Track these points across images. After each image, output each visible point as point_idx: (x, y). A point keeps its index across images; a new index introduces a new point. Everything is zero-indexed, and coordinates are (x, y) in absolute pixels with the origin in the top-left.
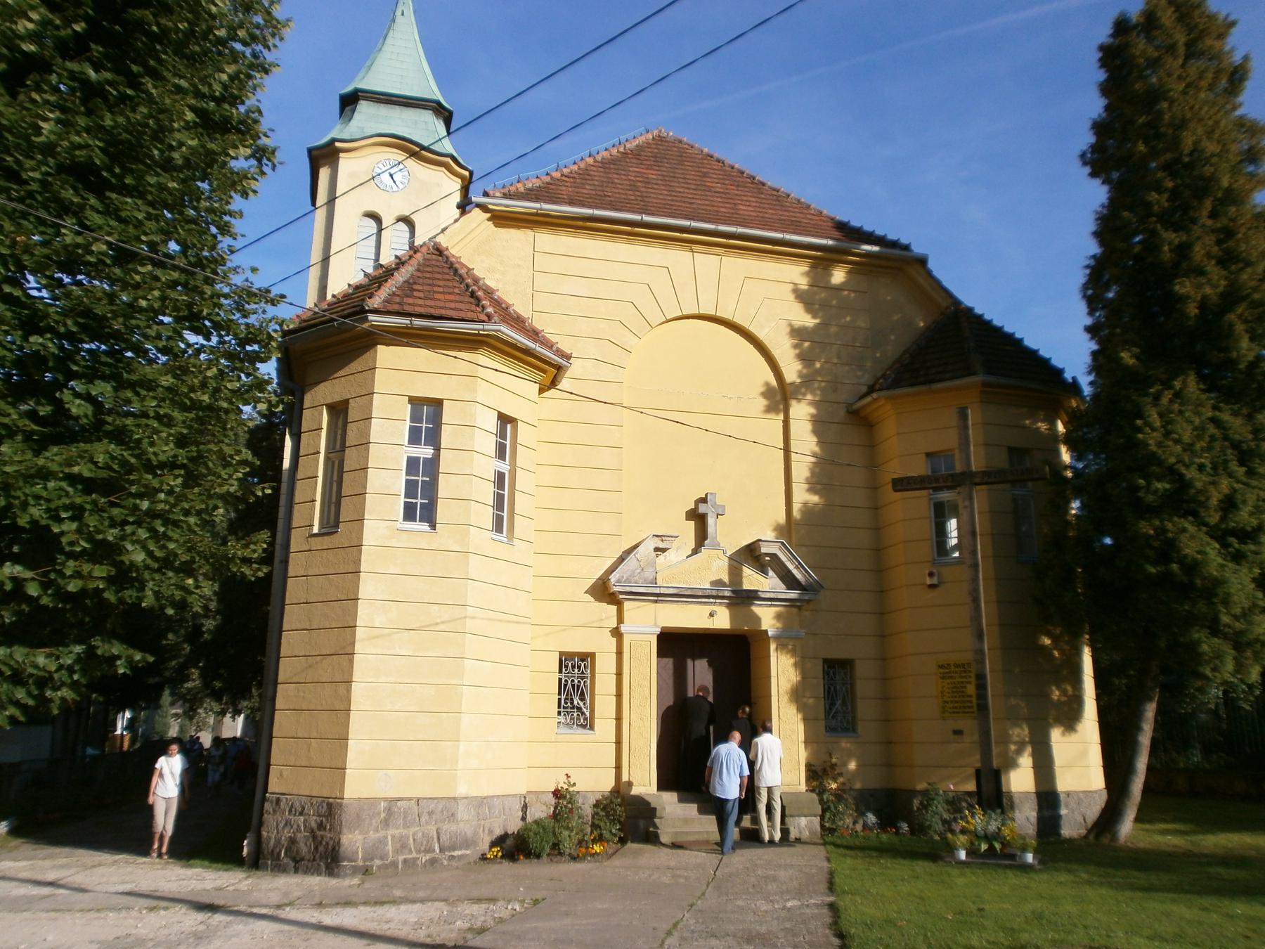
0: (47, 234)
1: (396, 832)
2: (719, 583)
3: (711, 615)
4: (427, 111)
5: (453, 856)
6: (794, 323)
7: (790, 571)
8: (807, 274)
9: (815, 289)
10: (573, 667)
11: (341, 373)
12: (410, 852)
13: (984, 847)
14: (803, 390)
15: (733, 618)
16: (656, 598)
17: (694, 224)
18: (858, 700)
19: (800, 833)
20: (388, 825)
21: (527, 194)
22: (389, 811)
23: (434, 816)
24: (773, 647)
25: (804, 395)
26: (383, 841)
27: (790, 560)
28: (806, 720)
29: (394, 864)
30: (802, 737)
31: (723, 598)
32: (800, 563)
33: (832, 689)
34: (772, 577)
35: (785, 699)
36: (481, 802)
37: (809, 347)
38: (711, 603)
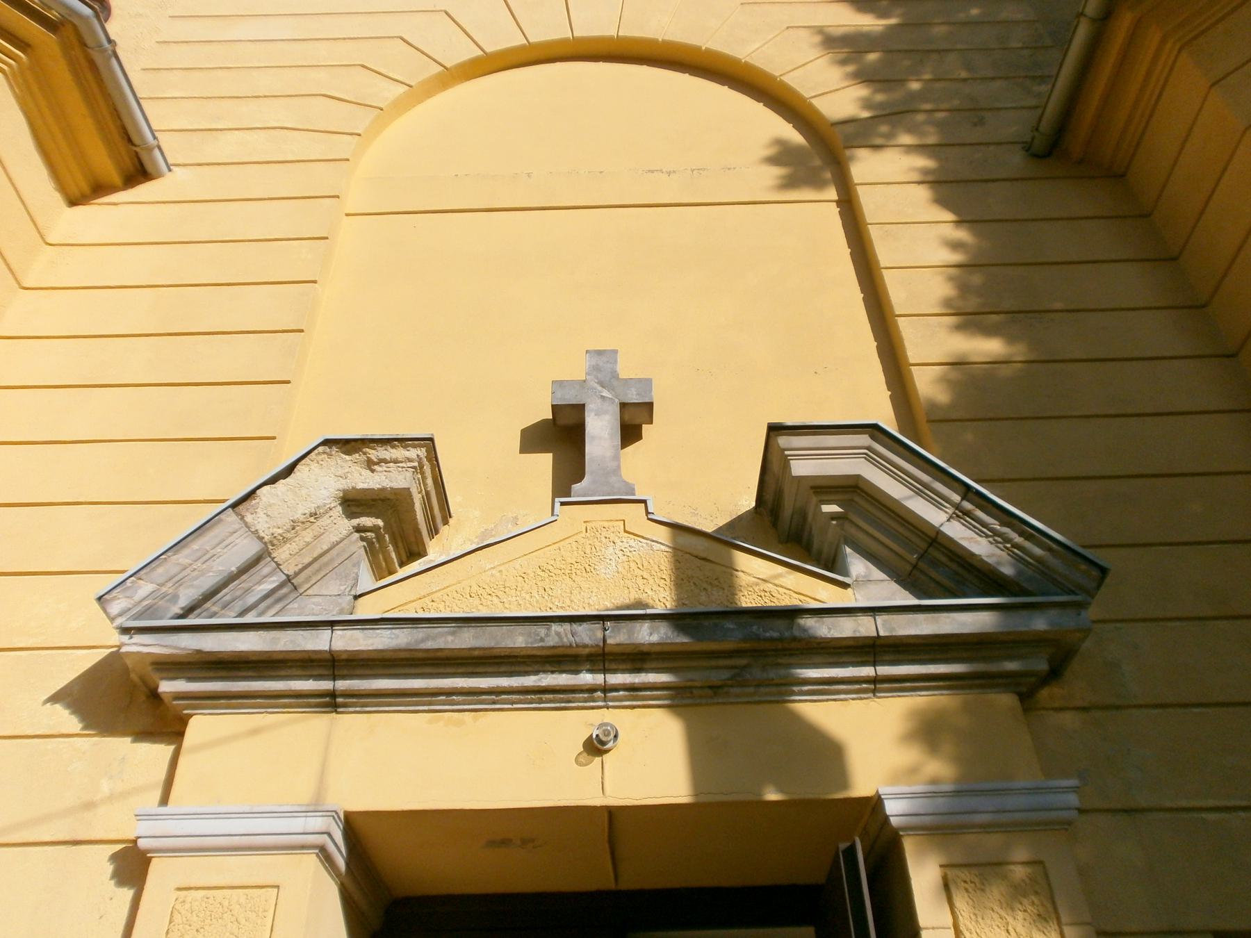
0: (314, 604)
3: (595, 747)
16: (326, 685)
27: (922, 490)
31: (637, 658)
32: (967, 491)
38: (591, 690)
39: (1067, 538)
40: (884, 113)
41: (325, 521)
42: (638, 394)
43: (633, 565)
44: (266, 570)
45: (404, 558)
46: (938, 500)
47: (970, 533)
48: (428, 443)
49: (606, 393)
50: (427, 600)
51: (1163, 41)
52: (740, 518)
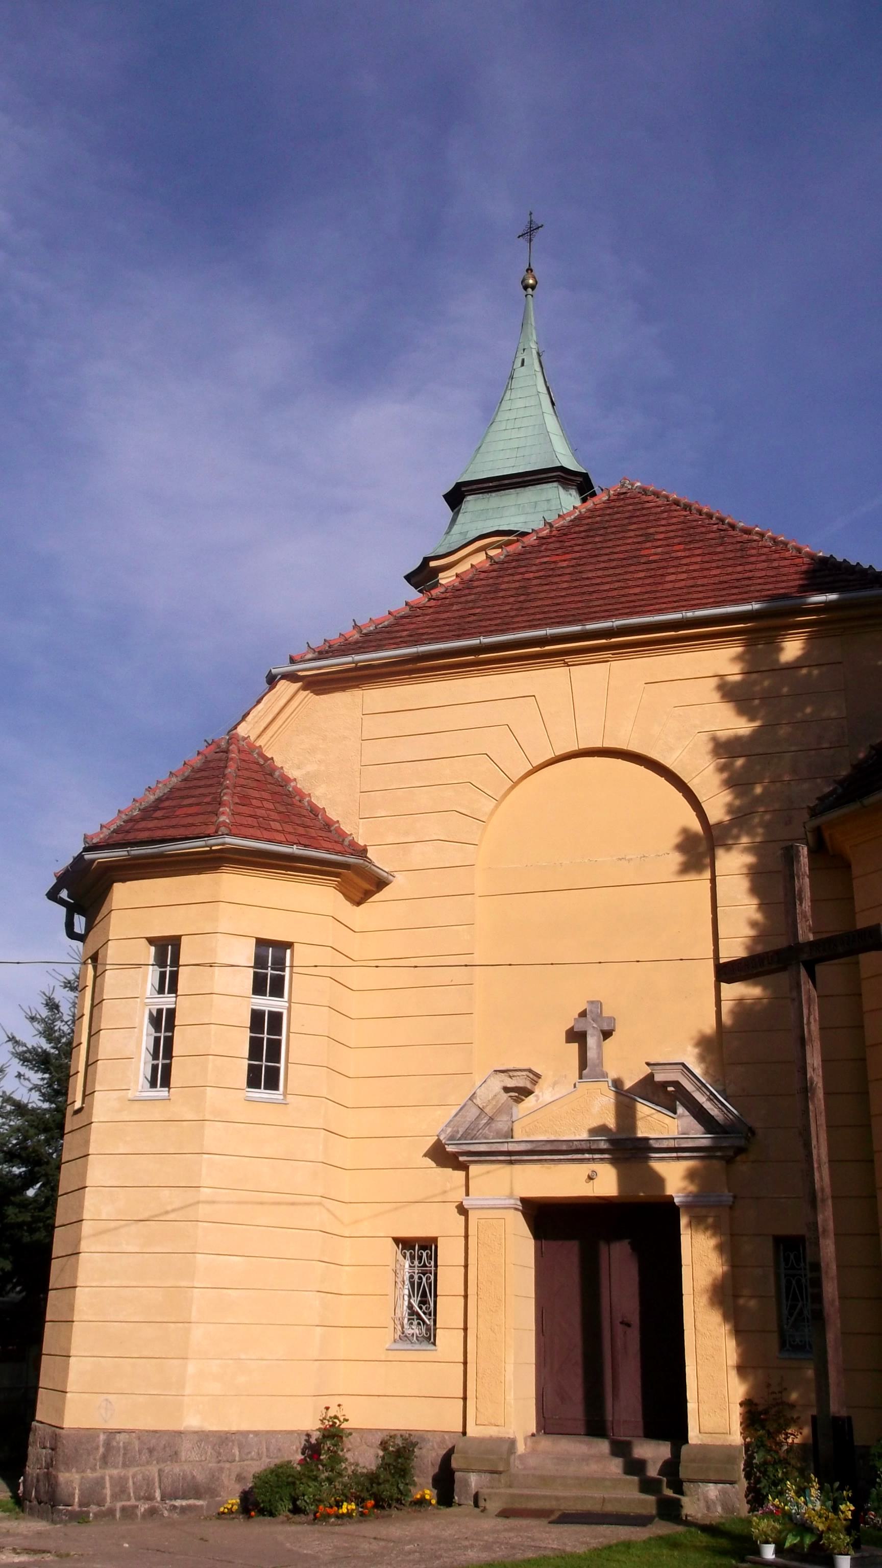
1: (115, 1472)
2: (602, 1130)
4: (550, 485)
5: (175, 1507)
6: (719, 734)
8: (739, 658)
9: (754, 676)
11: (98, 919)
12: (129, 1499)
14: (735, 831)
16: (508, 1158)
19: (708, 1508)
20: (106, 1463)
21: (364, 642)
22: (108, 1445)
23: (155, 1453)
24: (684, 1221)
25: (737, 837)
26: (100, 1482)
27: (699, 1089)
28: (739, 1333)
29: (111, 1512)
32: (711, 1093)
35: (704, 1300)
36: (223, 1440)
37: (744, 766)
38: (589, 1159)
40: (740, 815)
41: (499, 1096)
44: (483, 1116)
46: (703, 1094)
47: (712, 1107)
49: (595, 1025)
50: (536, 1123)
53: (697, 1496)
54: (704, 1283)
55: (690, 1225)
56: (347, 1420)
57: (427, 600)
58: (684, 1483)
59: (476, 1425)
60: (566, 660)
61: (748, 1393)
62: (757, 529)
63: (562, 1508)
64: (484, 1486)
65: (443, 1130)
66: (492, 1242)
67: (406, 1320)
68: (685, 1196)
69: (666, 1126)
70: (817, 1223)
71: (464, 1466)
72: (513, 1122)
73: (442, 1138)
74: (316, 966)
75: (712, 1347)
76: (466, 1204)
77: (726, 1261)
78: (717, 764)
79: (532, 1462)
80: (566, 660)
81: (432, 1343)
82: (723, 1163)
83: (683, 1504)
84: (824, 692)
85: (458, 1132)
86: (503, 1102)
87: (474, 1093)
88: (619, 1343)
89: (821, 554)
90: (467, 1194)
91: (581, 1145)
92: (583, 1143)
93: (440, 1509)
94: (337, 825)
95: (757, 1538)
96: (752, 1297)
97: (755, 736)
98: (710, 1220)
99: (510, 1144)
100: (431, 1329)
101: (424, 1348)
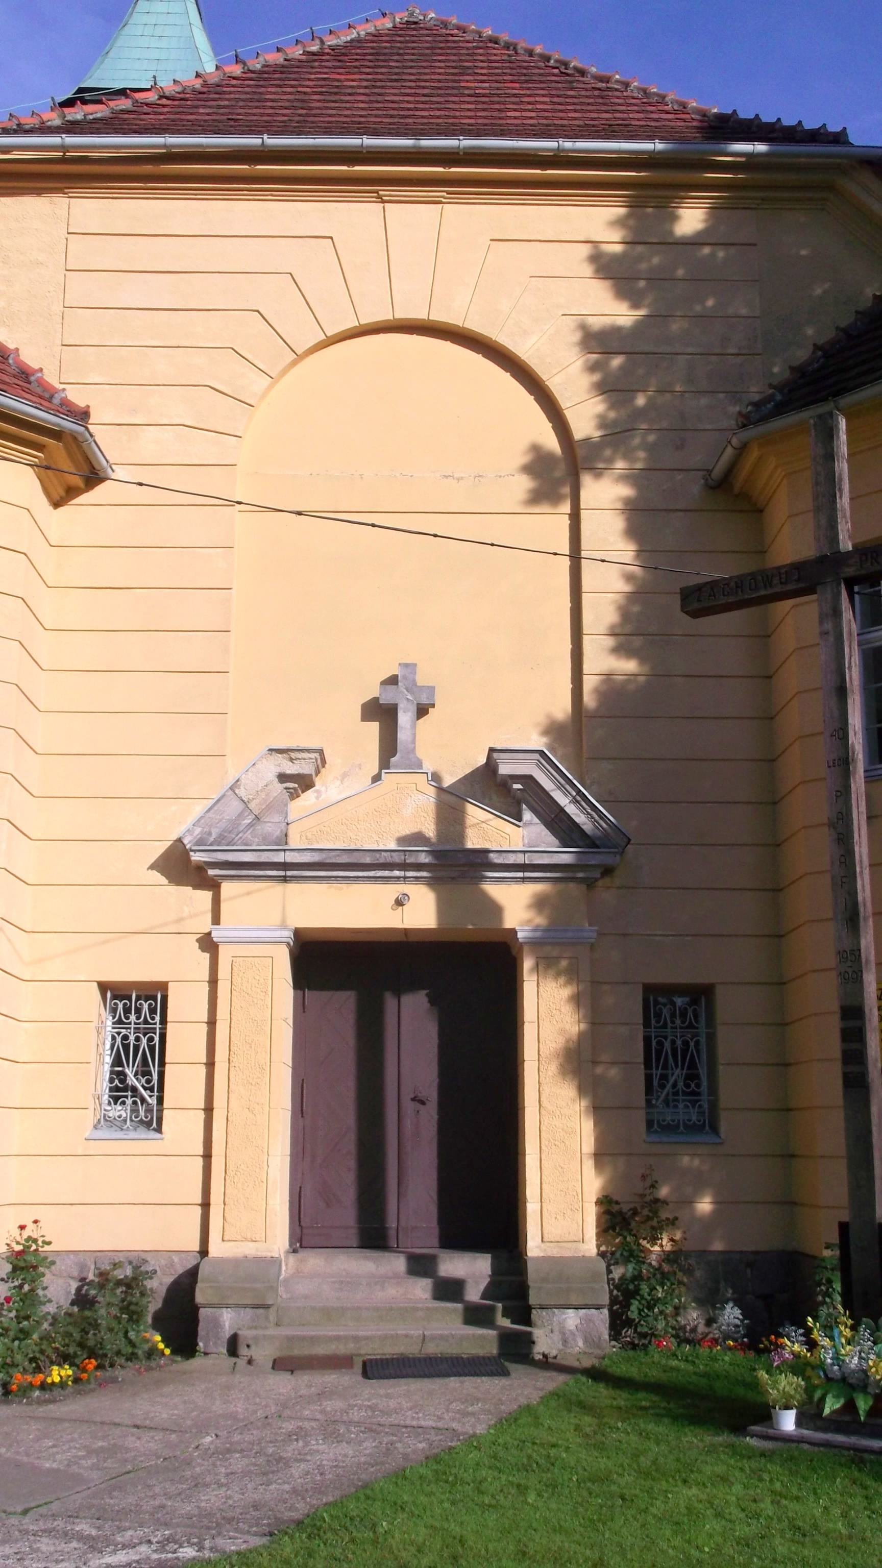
2: (418, 838)
3: (399, 903)
6: (591, 321)
7: (562, 810)
8: (620, 222)
9: (640, 248)
10: (127, 1011)
13: (831, 1405)
14: (608, 452)
15: (443, 908)
16: (282, 873)
17: (369, 141)
18: (721, 1067)
19: (565, 1342)
24: (528, 964)
25: (611, 460)
27: (560, 787)
28: (598, 1110)
30: (589, 1145)
31: (419, 867)
32: (579, 792)
33: (692, 1044)
34: (530, 823)
35: (552, 1069)
37: (621, 368)
38: (398, 878)
39: (617, 821)
41: (270, 787)
42: (427, 698)
43: (419, 809)
44: (246, 814)
45: (304, 788)
46: (566, 793)
47: (578, 811)
48: (321, 752)
49: (409, 697)
51: (776, 467)
52: (477, 769)
53: (550, 1327)
54: (554, 1045)
55: (536, 968)
56: (49, 1243)
57: (157, 97)
58: (534, 1311)
59: (223, 1240)
60: (381, 193)
61: (604, 1188)
62: (617, 77)
63: (363, 1352)
64: (244, 1326)
65: (189, 830)
66: (253, 989)
67: (106, 1097)
68: (533, 931)
69: (508, 837)
70: (859, 950)
71: (215, 1301)
72: (288, 824)
73: (186, 841)
74: (141, 484)
75: (563, 1130)
76: (216, 935)
77: (585, 1017)
78: (587, 360)
79: (301, 1288)
80: (381, 193)
81: (154, 1130)
82: (584, 887)
83: (535, 1339)
84: (733, 281)
85: (210, 834)
86: (275, 794)
87: (238, 781)
88: (408, 1124)
89: (716, 110)
90: (216, 920)
91: (391, 857)
92: (394, 854)
93: (176, 1362)
94: (39, 375)
95: (775, 1402)
96: (613, 1063)
97: (639, 328)
98: (564, 963)
99: (288, 853)
100: (153, 1110)
101: (143, 1136)
